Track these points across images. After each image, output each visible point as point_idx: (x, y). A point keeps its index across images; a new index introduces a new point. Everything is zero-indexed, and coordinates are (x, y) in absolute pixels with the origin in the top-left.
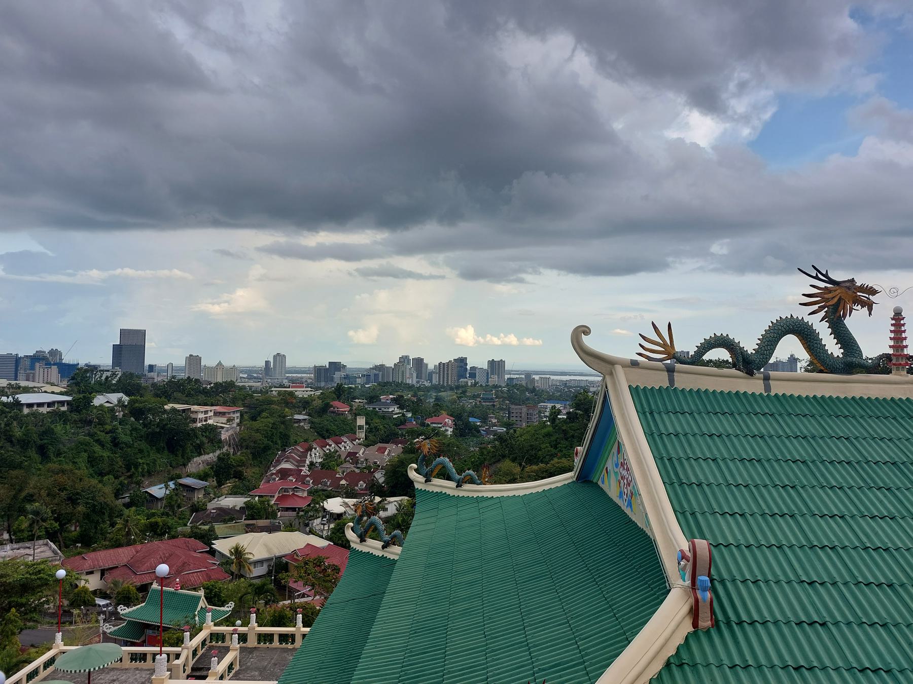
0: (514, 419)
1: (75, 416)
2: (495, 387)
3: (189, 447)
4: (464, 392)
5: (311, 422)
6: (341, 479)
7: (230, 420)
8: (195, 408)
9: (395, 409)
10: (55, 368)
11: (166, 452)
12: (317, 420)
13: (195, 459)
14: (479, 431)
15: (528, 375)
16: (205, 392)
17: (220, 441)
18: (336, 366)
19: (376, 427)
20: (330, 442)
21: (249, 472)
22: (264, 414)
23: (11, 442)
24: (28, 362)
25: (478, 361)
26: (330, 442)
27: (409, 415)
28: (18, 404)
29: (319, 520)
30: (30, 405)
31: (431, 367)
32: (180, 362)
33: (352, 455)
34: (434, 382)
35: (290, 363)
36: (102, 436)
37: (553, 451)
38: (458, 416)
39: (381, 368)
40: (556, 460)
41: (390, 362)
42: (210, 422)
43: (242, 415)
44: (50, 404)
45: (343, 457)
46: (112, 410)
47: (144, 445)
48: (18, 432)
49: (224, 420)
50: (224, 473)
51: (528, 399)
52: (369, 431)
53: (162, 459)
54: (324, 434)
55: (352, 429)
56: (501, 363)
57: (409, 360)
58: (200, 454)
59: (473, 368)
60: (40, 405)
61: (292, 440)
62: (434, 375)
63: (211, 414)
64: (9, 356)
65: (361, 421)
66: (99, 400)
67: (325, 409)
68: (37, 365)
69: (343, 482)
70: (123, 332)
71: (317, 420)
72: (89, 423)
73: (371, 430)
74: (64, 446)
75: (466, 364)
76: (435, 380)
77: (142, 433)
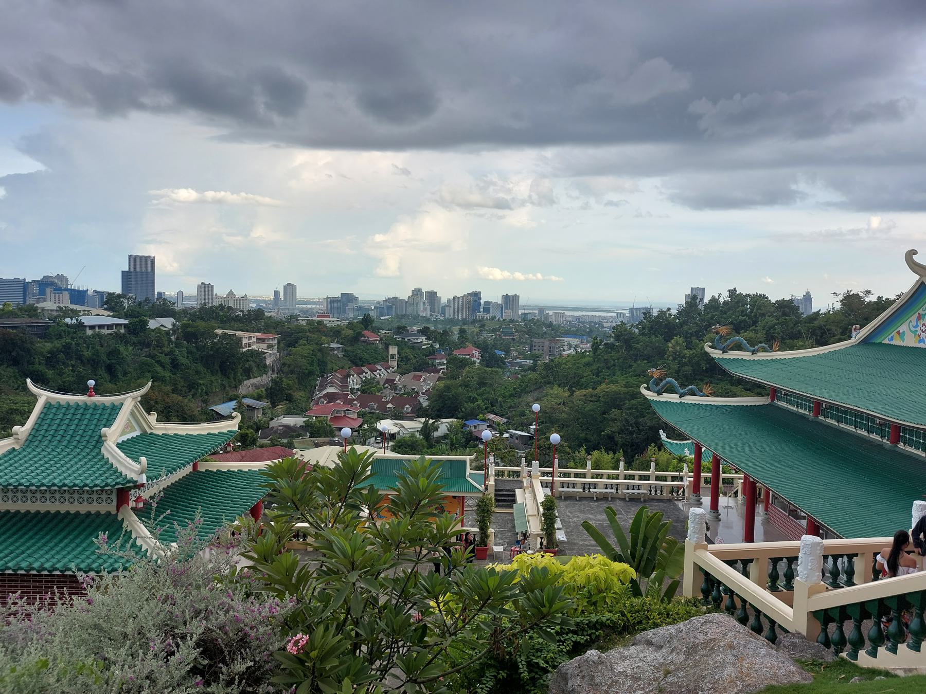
0: (537, 352)
1: (134, 339)
2: (512, 321)
3: (240, 371)
4: (483, 326)
5: (344, 350)
6: (388, 403)
7: (270, 347)
8: (239, 333)
9: (422, 339)
10: (66, 294)
11: (219, 374)
12: (349, 348)
13: (245, 382)
14: (504, 363)
15: (542, 310)
16: (238, 319)
17: (265, 366)
18: (348, 298)
19: (406, 357)
20: (366, 370)
21: (298, 395)
22: (301, 342)
23: (82, 361)
24: (36, 289)
25: (491, 295)
26: (366, 370)
27: (438, 346)
28: (81, 325)
29: (373, 439)
30: (92, 327)
31: (444, 300)
32: (191, 290)
33: (390, 381)
34: (447, 316)
35: (301, 294)
36: (163, 358)
37: (596, 379)
38: (484, 348)
39: (394, 301)
40: (604, 385)
41: (404, 295)
42: (254, 347)
43: (279, 342)
44: (109, 327)
45: (382, 383)
46: (167, 333)
47: (200, 368)
48: (87, 354)
49: (265, 346)
50: (276, 395)
51: (545, 333)
52: (401, 360)
53: (218, 380)
54: (358, 362)
55: (383, 358)
56: (516, 298)
57: (422, 293)
58: (249, 378)
59: (487, 303)
60: (101, 327)
61: (329, 367)
62: (447, 309)
63: (254, 340)
64: (16, 281)
65: (393, 350)
66: (153, 324)
67: (356, 339)
68: (48, 290)
69: (390, 405)
70: (131, 258)
71: (349, 348)
72: (148, 345)
73: (403, 359)
74: (129, 366)
75: (480, 299)
76: (449, 314)
77: (197, 356)
